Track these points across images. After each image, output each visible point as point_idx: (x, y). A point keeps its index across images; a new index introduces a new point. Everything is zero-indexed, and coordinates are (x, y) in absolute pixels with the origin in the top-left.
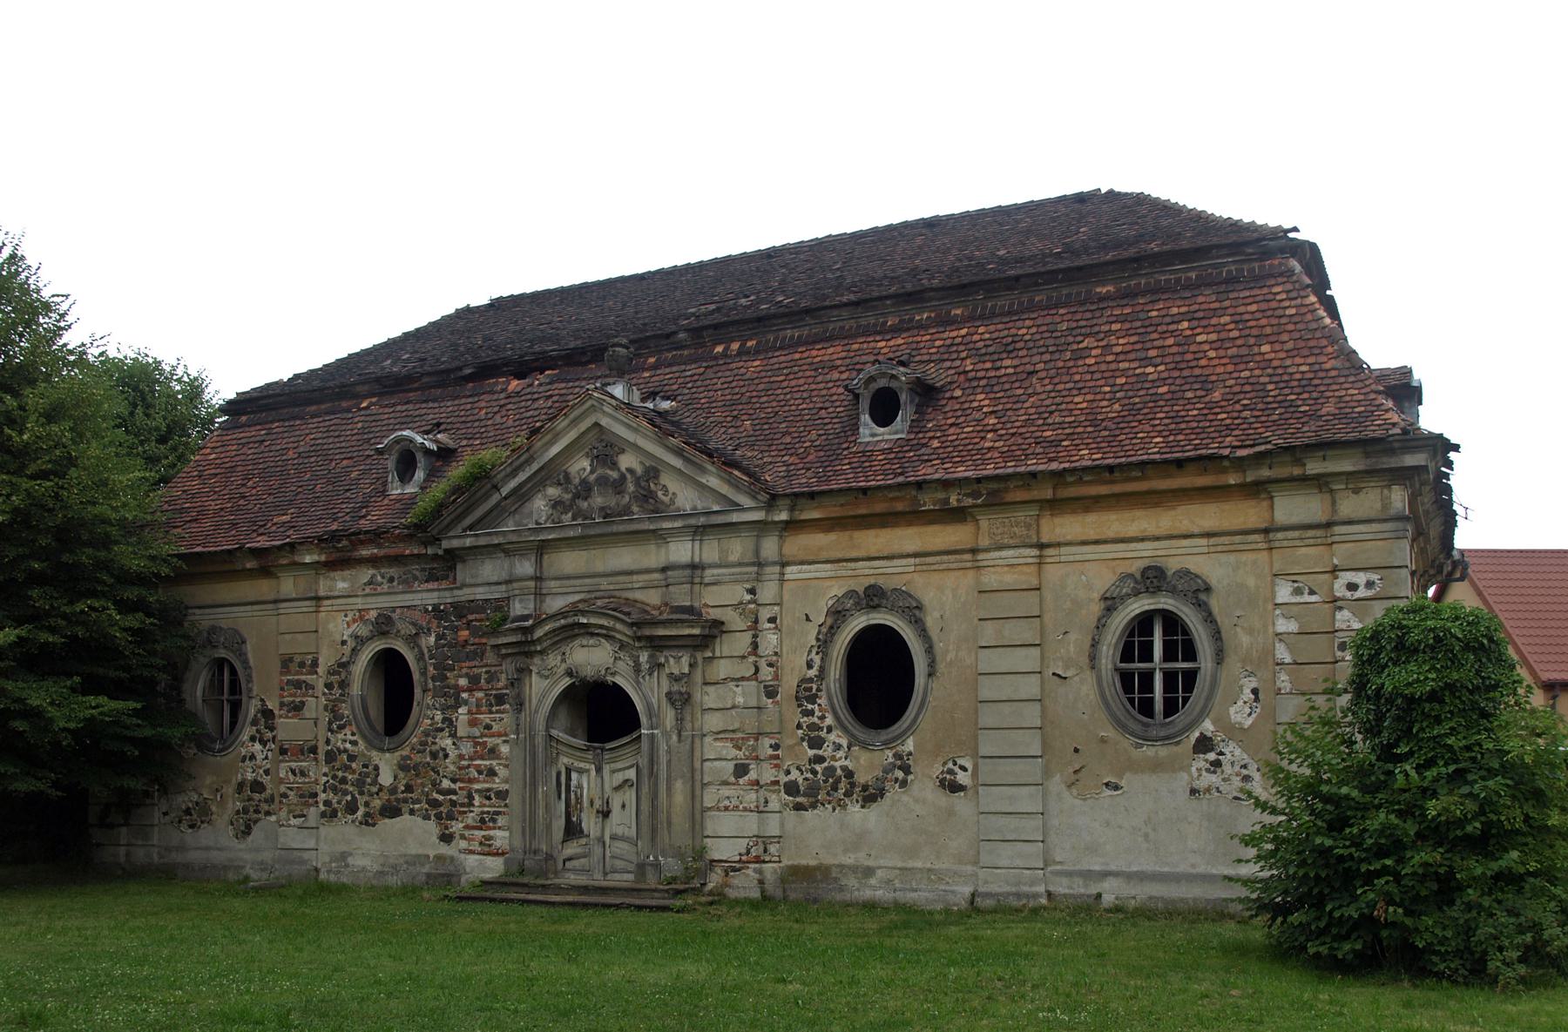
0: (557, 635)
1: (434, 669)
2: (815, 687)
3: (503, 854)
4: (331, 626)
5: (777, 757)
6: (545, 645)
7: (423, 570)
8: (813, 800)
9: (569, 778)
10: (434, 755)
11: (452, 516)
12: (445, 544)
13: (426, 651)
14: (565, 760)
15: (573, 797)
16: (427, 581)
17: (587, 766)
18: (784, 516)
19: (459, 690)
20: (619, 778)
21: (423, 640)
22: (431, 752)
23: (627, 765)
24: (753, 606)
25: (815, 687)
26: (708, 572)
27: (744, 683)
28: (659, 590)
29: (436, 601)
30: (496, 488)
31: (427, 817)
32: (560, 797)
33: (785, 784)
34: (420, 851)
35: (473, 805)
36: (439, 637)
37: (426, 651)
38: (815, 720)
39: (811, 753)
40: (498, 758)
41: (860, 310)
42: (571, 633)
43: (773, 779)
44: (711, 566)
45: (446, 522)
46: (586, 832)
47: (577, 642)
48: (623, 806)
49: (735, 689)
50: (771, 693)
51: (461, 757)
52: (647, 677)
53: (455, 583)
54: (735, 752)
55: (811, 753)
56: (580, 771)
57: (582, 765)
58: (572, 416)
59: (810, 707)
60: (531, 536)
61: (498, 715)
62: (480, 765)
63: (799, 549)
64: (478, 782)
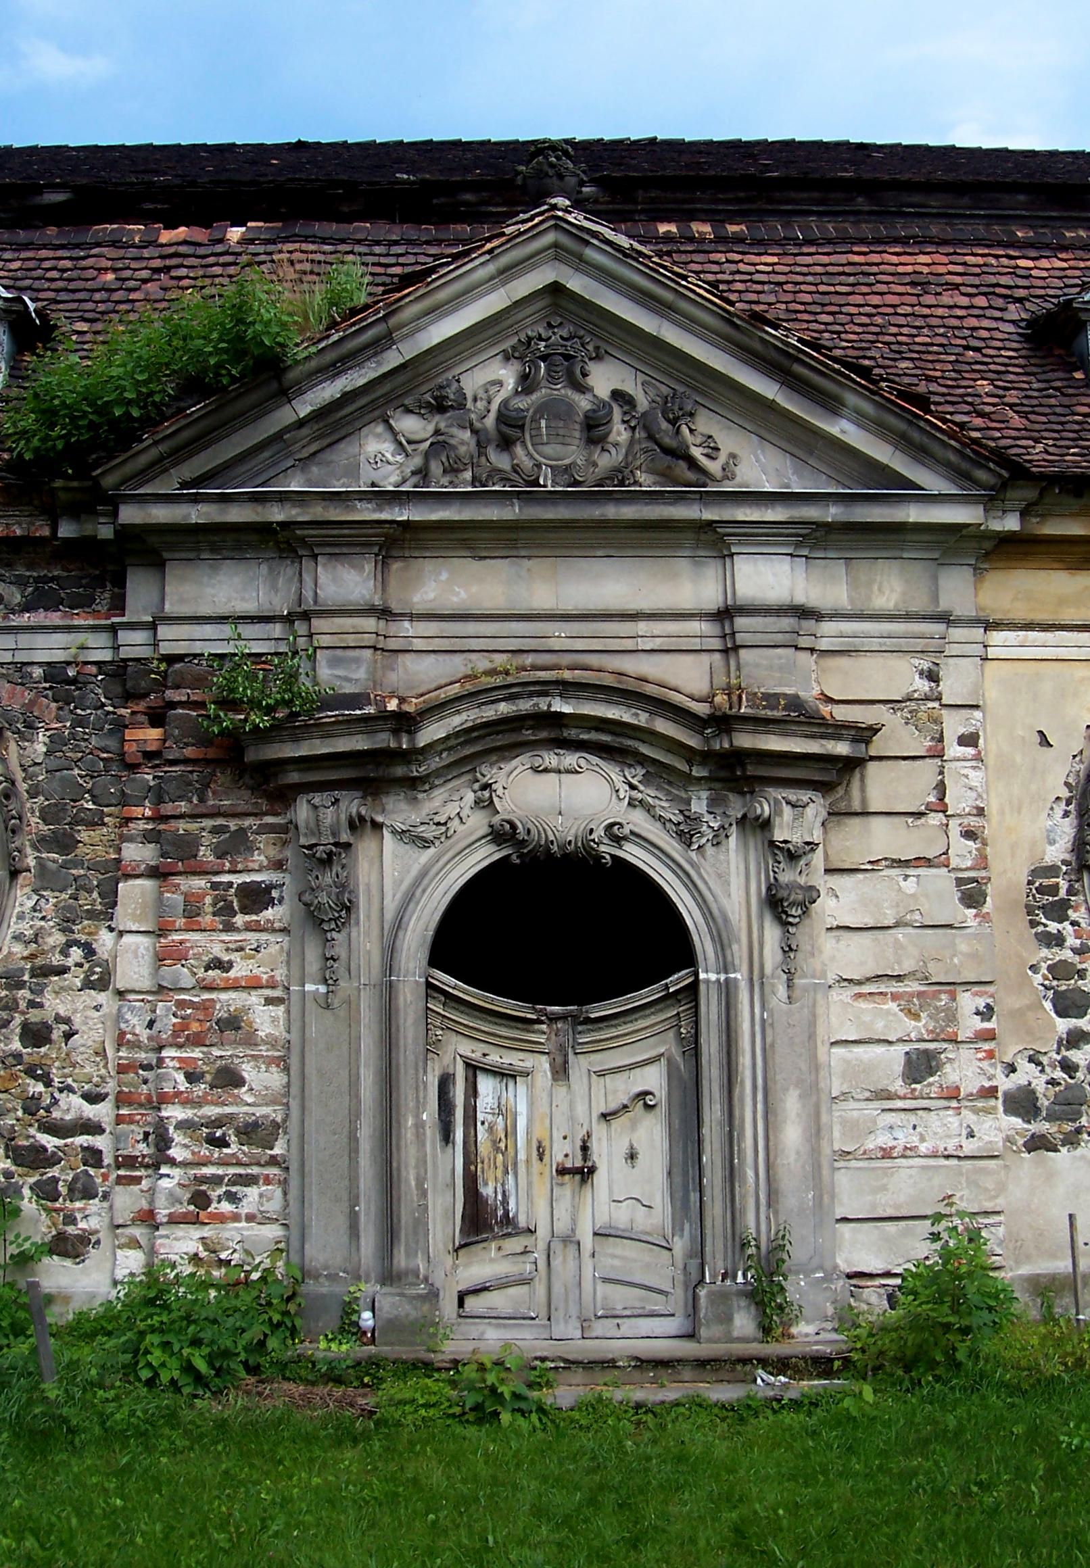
4: (433, 584)
5: (989, 1036)
6: (435, 763)
8: (1069, 1127)
12: (129, 514)
13: (19, 775)
14: (466, 1048)
18: (1011, 523)
20: (622, 1089)
21: (13, 746)
22: (25, 1026)
26: (827, 627)
27: (920, 871)
28: (705, 658)
29: (59, 656)
30: (285, 394)
32: (447, 1136)
33: (1006, 1094)
37: (19, 775)
38: (1067, 955)
39: (1063, 1025)
41: (965, 201)
44: (836, 615)
46: (522, 1222)
48: (632, 1156)
50: (973, 897)
55: (1063, 1025)
56: (505, 1075)
58: (504, 260)
59: (1053, 927)
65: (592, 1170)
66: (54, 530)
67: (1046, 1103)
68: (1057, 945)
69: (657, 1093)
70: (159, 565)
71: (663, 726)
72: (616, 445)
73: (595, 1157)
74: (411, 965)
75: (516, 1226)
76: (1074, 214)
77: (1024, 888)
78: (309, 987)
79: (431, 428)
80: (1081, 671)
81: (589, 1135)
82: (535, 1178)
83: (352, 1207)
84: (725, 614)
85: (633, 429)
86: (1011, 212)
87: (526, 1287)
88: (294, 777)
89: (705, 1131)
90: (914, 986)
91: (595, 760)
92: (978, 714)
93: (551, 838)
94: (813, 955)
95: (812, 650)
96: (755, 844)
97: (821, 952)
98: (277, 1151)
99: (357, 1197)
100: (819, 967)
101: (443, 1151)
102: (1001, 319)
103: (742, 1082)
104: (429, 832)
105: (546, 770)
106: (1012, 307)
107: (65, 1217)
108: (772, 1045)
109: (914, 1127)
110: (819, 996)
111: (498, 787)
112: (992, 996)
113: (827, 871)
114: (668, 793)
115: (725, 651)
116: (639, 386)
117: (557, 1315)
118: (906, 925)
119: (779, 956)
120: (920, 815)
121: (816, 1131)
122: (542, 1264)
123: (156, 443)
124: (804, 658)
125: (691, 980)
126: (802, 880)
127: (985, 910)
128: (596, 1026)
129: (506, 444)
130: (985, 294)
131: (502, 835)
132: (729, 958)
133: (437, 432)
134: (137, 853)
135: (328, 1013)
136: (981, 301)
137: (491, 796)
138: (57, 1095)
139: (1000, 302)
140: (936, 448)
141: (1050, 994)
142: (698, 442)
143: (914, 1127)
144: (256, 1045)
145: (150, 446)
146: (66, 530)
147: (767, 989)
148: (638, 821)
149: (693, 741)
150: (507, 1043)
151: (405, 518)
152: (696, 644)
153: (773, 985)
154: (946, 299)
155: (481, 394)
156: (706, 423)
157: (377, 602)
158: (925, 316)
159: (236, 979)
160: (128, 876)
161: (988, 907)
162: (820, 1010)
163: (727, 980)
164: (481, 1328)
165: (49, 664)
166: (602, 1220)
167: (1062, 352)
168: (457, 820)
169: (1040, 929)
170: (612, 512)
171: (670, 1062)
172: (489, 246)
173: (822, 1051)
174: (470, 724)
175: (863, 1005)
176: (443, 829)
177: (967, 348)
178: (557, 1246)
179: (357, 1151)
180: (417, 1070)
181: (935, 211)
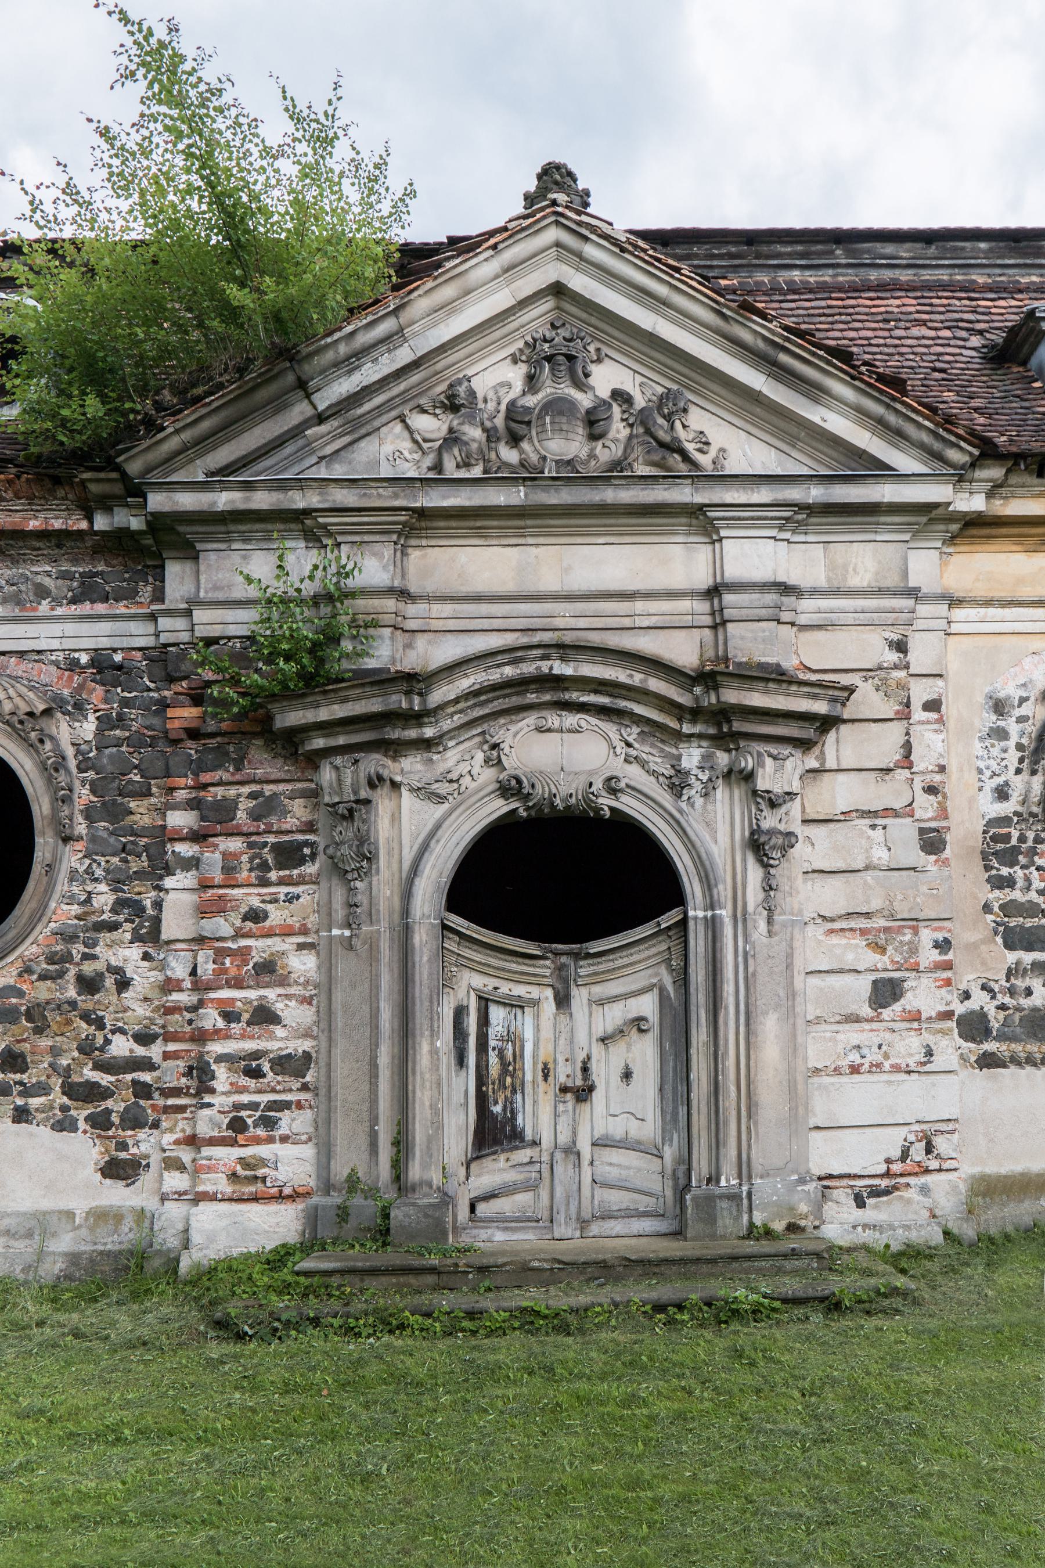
0: (482, 704)
1: (93, 791)
2: (1015, 834)
3: (295, 1196)
5: (948, 966)
6: (447, 724)
7: (64, 576)
9: (484, 1021)
10: (89, 985)
11: (186, 436)
12: (157, 501)
13: (70, 752)
14: (478, 981)
15: (493, 1059)
16: (74, 601)
17: (535, 992)
19: (163, 835)
20: (615, 1015)
23: (634, 987)
24: (901, 674)
25: (1015, 834)
26: (806, 604)
29: (105, 643)
31: (65, 1125)
32: (461, 1061)
34: (47, 1204)
35: (212, 1091)
36: (105, 723)
37: (70, 752)
40: (283, 981)
41: (932, 250)
42: (515, 701)
43: (943, 1008)
44: (815, 592)
45: (168, 447)
46: (529, 1135)
47: (531, 719)
48: (627, 1075)
49: (870, 832)
51: (169, 986)
52: (699, 801)
53: (163, 601)
54: (871, 958)
57: (520, 990)
59: (1005, 871)
60: (396, 496)
61: (284, 890)
62: (233, 1000)
63: (977, 580)
64: (228, 1037)
65: (591, 1089)
66: (91, 522)
67: (997, 1025)
68: (1008, 886)
69: (651, 1019)
70: (191, 554)
71: (656, 685)
72: (615, 441)
73: (594, 1077)
74: (426, 911)
75: (522, 1140)
76: (1028, 261)
77: (980, 836)
78: (336, 932)
79: (445, 428)
80: (1036, 643)
81: (589, 1058)
82: (541, 1095)
83: (372, 1128)
84: (714, 592)
85: (631, 426)
86: (973, 261)
87: (531, 1194)
88: (319, 743)
89: (693, 1051)
90: (882, 923)
91: (594, 721)
92: (940, 682)
93: (554, 791)
94: (791, 895)
95: (793, 624)
96: (739, 792)
97: (798, 893)
98: (308, 1078)
99: (376, 1118)
100: (796, 906)
101: (457, 1076)
102: (965, 347)
103: (726, 1008)
104: (443, 788)
105: (549, 730)
106: (973, 338)
107: (117, 1143)
108: (754, 974)
109: (880, 1047)
110: (796, 931)
111: (505, 746)
112: (950, 931)
113: (804, 821)
114: (662, 750)
115: (714, 627)
116: (637, 388)
117: (561, 1218)
118: (875, 868)
119: (761, 895)
120: (889, 770)
121: (792, 1047)
122: (546, 1174)
123: (177, 431)
124: (786, 631)
125: (681, 917)
126: (782, 827)
127: (944, 856)
128: (596, 960)
129: (515, 440)
130: (949, 328)
131: (511, 788)
132: (716, 897)
133: (451, 430)
134: (179, 819)
135: (352, 954)
136: (947, 333)
137: (499, 756)
138: (109, 1036)
139: (964, 334)
140: (910, 430)
141: (1002, 929)
142: (690, 438)
143: (880, 1047)
144: (289, 985)
145: (172, 434)
146: (101, 523)
147: (750, 924)
148: (634, 774)
149: (683, 698)
150: (517, 977)
151: (418, 505)
152: (688, 620)
153: (755, 921)
154: (915, 331)
155: (491, 395)
156: (698, 419)
157: (396, 584)
158: (896, 346)
159: (271, 927)
160: (173, 840)
161: (948, 853)
162: (797, 944)
163: (713, 917)
164: (490, 1231)
165: (96, 650)
166: (599, 1131)
167: (1021, 369)
168: (468, 778)
169: (994, 872)
170: (610, 495)
171: (662, 990)
172: (492, 241)
173: (799, 980)
174: (477, 687)
175: (835, 940)
176: (456, 785)
177: (935, 370)
178: (559, 1156)
179: (377, 1077)
180: (431, 1002)
181: (904, 262)
